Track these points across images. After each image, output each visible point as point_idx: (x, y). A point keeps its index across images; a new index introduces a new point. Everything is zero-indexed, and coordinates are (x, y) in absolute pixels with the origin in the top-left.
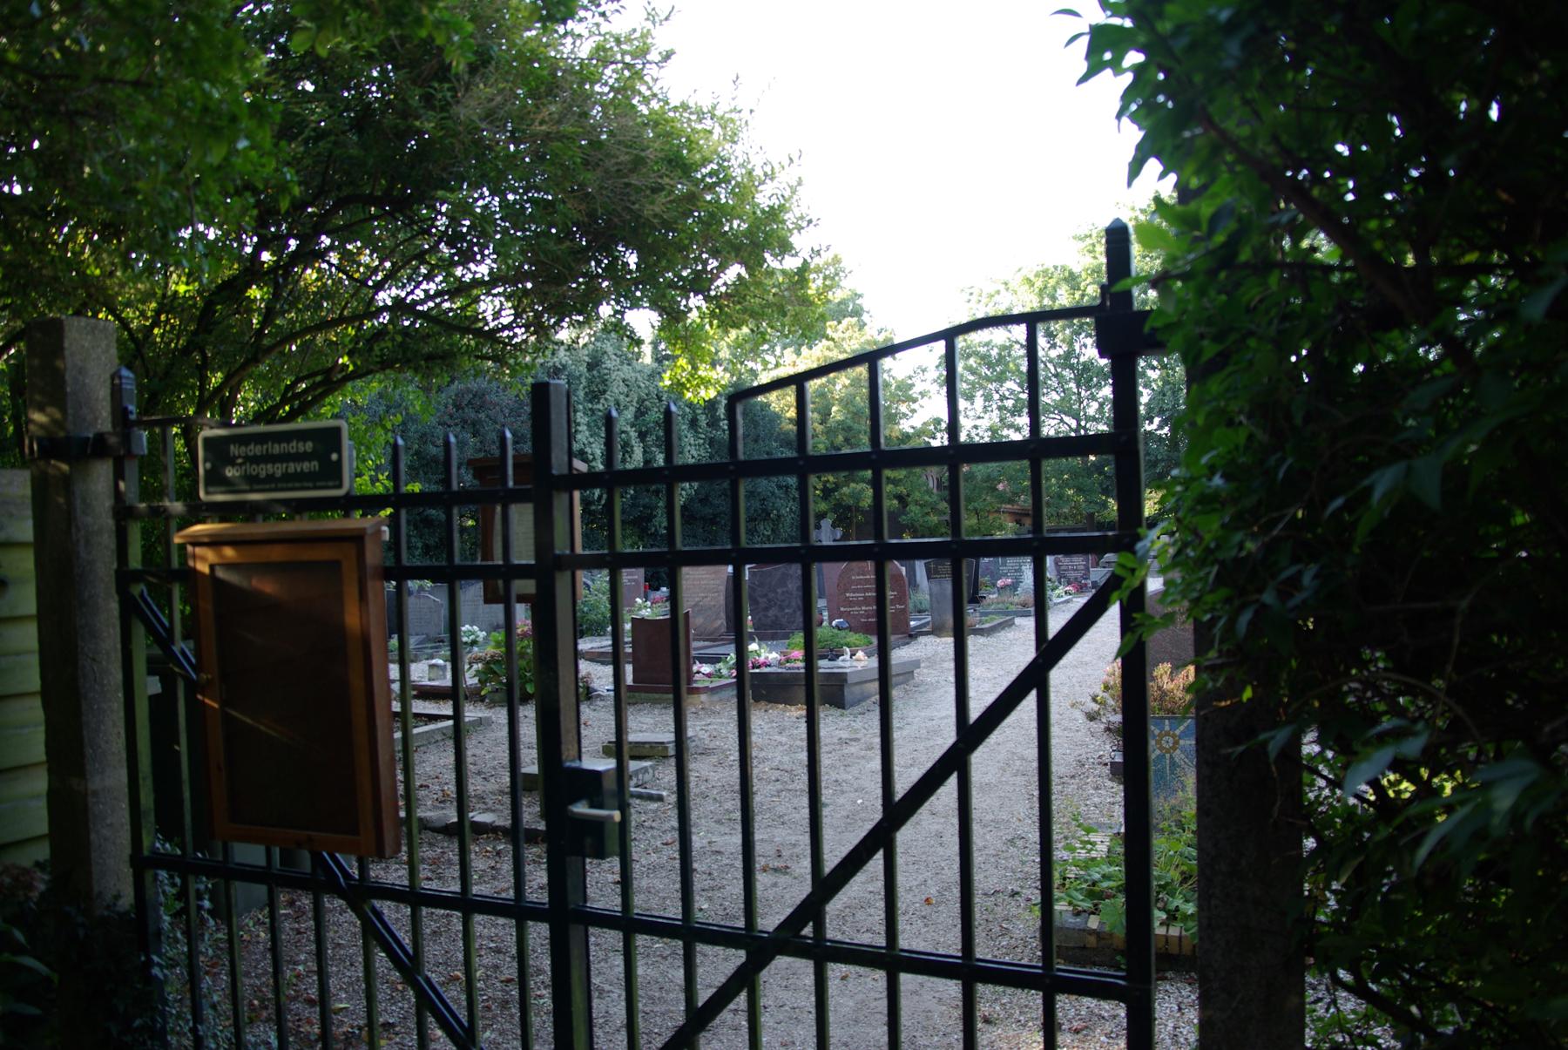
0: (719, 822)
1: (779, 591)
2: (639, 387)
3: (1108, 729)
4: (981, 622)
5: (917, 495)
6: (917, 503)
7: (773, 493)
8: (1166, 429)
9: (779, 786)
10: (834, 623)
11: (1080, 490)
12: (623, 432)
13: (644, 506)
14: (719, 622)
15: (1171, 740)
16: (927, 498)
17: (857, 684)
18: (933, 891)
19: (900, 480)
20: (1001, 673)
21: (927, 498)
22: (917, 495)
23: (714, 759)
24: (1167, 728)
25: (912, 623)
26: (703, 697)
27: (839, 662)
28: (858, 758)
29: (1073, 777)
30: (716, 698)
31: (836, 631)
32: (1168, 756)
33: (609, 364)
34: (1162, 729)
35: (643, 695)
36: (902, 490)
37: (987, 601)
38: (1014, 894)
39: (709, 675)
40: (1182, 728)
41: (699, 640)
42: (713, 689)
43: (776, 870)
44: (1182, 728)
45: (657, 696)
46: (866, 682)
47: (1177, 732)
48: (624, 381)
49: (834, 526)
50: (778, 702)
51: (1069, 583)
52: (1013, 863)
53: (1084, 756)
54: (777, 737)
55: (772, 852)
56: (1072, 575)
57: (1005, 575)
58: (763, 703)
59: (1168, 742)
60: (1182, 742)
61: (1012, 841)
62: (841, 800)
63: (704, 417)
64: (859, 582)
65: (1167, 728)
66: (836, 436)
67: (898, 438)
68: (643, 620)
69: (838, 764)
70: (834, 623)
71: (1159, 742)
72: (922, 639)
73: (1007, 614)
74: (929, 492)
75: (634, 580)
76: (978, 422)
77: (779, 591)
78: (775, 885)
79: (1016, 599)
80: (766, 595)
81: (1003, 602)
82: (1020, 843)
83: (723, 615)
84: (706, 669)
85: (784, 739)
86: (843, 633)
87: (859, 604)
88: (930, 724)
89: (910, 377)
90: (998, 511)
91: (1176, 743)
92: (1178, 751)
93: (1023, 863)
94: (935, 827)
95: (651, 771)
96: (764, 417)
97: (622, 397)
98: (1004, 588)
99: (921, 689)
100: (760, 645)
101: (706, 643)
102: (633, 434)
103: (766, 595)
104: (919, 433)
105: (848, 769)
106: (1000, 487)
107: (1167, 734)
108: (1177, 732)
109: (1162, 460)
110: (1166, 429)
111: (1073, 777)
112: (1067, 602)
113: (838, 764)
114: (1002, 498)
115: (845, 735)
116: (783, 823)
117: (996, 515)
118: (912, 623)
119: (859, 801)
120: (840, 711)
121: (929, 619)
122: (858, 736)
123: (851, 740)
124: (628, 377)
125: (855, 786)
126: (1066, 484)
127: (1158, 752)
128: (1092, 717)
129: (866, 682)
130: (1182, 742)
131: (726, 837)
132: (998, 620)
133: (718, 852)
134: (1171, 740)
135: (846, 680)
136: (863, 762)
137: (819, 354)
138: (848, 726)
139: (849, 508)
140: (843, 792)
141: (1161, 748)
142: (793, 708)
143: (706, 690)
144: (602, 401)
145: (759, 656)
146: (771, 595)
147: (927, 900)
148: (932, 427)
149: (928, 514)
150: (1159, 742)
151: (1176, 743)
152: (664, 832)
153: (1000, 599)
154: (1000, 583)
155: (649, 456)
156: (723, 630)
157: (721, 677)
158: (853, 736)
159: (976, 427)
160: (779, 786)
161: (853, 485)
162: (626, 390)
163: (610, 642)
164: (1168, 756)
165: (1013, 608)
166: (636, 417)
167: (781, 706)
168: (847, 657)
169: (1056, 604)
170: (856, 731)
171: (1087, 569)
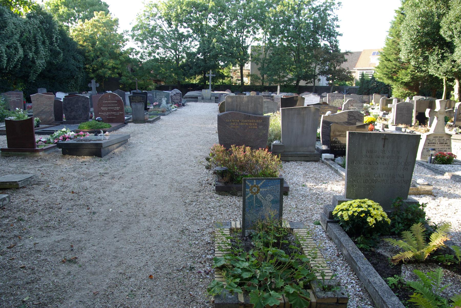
0: (41, 229)
1: (75, 106)
2: (21, 27)
3: (215, 173)
4: (149, 118)
5: (125, 73)
6: (125, 76)
7: (75, 70)
8: (203, 57)
9: (72, 203)
10: (97, 119)
11: (176, 74)
12: (15, 43)
13: (25, 72)
14: (52, 117)
15: (256, 189)
16: (128, 74)
17: (106, 147)
18: (152, 270)
19: (119, 68)
20: (160, 139)
21: (128, 74)
22: (125, 73)
23: (42, 187)
24: (255, 184)
25: (125, 118)
26: (41, 153)
27: (99, 137)
28: (108, 184)
29: (199, 191)
30: (46, 153)
31: (97, 122)
32: (255, 196)
33: (6, 16)
34: (253, 184)
35: (13, 153)
36: (119, 71)
37: (150, 110)
38: (192, 269)
39: (45, 142)
40: (261, 183)
41: (44, 124)
42: (45, 149)
43: (70, 261)
44: (261, 183)
45: (19, 153)
46: (110, 146)
47: (259, 185)
48: (14, 23)
49: (96, 82)
50: (73, 155)
51: (175, 104)
52: (186, 246)
53: (201, 180)
54: (72, 174)
55: (68, 248)
56: (176, 101)
57: (156, 101)
58: (67, 155)
59: (255, 190)
60: (261, 190)
61: (182, 231)
62: (102, 210)
63: (48, 41)
64: (106, 103)
65: (255, 184)
66: (97, 52)
67: (119, 54)
68: (11, 121)
69: (100, 188)
70: (97, 119)
71: (251, 190)
72: (129, 124)
73: (157, 115)
74: (128, 72)
75: (19, 100)
76: (145, 50)
77: (75, 106)
78: (69, 273)
79: (160, 110)
80: (70, 108)
81: (156, 111)
82: (186, 232)
83: (53, 115)
84: (44, 138)
85: (75, 174)
86: (100, 123)
87: (106, 111)
88: (137, 164)
89: (123, 34)
90: (150, 79)
91: (258, 190)
92: (259, 194)
93: (191, 245)
94: (147, 224)
95: (7, 199)
96: (71, 43)
97: (13, 30)
98: (156, 105)
99: (131, 146)
100: (66, 129)
101: (47, 126)
102: (19, 45)
103: (70, 108)
104: (126, 52)
105: (104, 190)
106: (151, 72)
107: (255, 186)
108: (259, 185)
109: (202, 66)
110: (203, 57)
111: (199, 191)
112: (176, 110)
113: (100, 188)
114: (152, 76)
115: (102, 171)
116: (74, 227)
117: (149, 81)
118: (125, 118)
119: (110, 210)
120: (99, 159)
121: (131, 116)
122: (108, 172)
123: (105, 173)
124: (15, 22)
125: (108, 200)
126: (172, 72)
127: (250, 194)
128: (208, 168)
129: (110, 146)
130: (261, 190)
131: (45, 239)
132: (155, 117)
133: (39, 251)
134: (256, 189)
135: (102, 146)
136: (110, 186)
137: (91, 22)
138: (104, 166)
139: (102, 76)
140: (102, 204)
141: (252, 192)
142: (80, 158)
143: (42, 150)
144: (5, 30)
145: (66, 133)
146: (72, 107)
147: (151, 276)
148: (130, 51)
149: (128, 79)
150: (251, 190)
151: (258, 190)
152: (10, 239)
153: (155, 109)
154: (154, 104)
155: (26, 54)
156: (54, 120)
157: (50, 143)
158: (106, 172)
159: (144, 52)
160: (72, 203)
161: (103, 69)
162: (15, 27)
163: (5, 125)
164: (255, 196)
165: (159, 113)
166: (20, 38)
167: (75, 157)
168: (102, 134)
169: (172, 111)
170: (107, 169)
171: (181, 100)
